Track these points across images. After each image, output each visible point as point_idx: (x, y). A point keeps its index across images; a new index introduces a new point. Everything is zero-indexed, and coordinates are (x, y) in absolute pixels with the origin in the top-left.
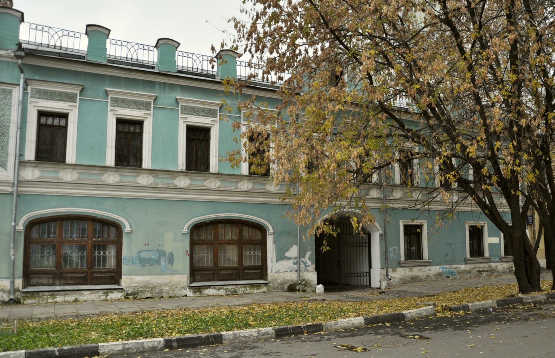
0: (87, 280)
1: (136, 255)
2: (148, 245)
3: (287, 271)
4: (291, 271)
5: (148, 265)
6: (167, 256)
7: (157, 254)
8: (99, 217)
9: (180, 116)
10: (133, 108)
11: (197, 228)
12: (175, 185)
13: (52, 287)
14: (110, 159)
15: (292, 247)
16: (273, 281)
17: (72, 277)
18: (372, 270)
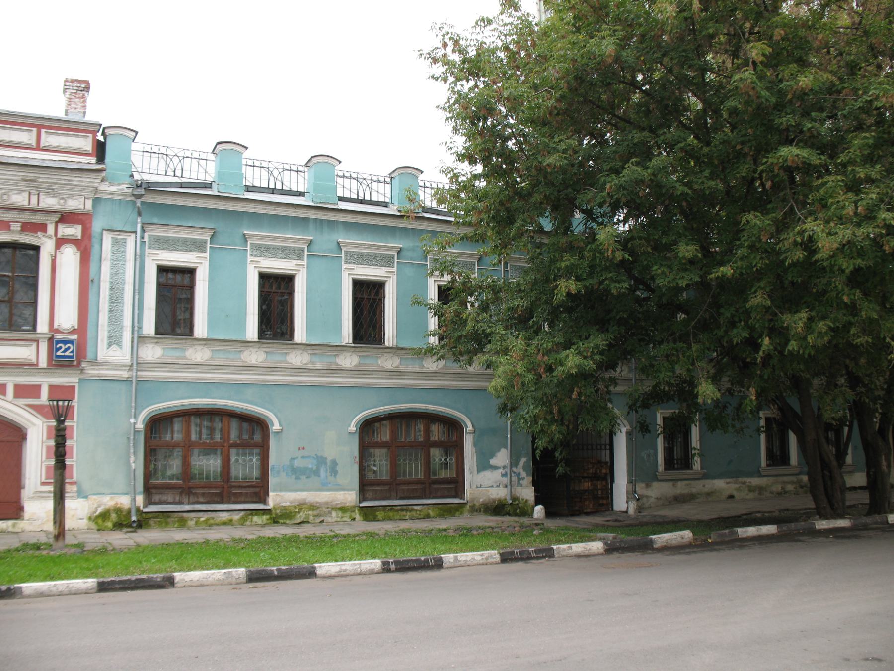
2: (304, 448)
6: (328, 464)
7: (315, 462)
8: (238, 411)
10: (181, 250)
11: (368, 426)
14: (252, 331)
15: (499, 451)
16: (473, 499)
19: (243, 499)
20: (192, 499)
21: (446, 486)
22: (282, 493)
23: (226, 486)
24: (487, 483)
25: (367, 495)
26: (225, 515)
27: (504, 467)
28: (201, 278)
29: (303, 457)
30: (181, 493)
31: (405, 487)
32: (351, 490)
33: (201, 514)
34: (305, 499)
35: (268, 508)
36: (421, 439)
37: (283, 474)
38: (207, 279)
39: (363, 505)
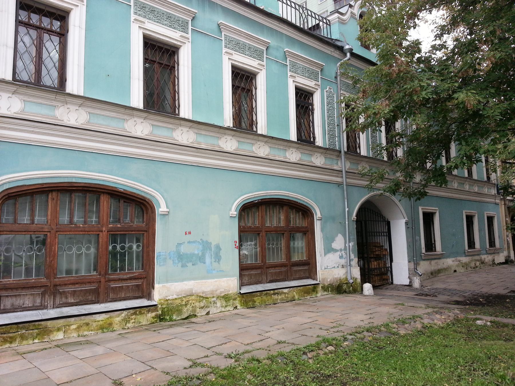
0: (99, 294)
1: (175, 249)
2: (190, 233)
3: (334, 267)
4: (338, 267)
5: (190, 265)
6: (213, 249)
7: (201, 247)
8: (121, 188)
9: (224, 50)
10: (165, 25)
11: (247, 209)
12: (220, 147)
13: (41, 312)
14: (137, 100)
15: (337, 236)
16: (324, 279)
17: (75, 291)
18: (393, 264)
19: (123, 296)
20: (58, 301)
21: (301, 268)
22: (168, 285)
23: (103, 280)
24: (331, 264)
25: (244, 281)
26: (103, 316)
27: (341, 250)
28: (77, 23)
29: (189, 242)
30: (43, 294)
31: (272, 270)
32: (233, 276)
33: (73, 319)
34: (192, 289)
35: (154, 303)
36: (282, 224)
37: (170, 262)
38: (84, 26)
39: (244, 290)
